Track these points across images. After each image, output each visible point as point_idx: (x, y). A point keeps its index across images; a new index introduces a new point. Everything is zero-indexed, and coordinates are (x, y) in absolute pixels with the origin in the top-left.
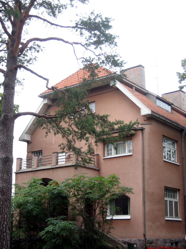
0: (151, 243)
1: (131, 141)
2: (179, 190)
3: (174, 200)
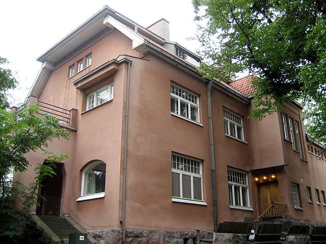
0: (137, 236)
1: (269, 189)
2: (202, 161)
3: (192, 175)
